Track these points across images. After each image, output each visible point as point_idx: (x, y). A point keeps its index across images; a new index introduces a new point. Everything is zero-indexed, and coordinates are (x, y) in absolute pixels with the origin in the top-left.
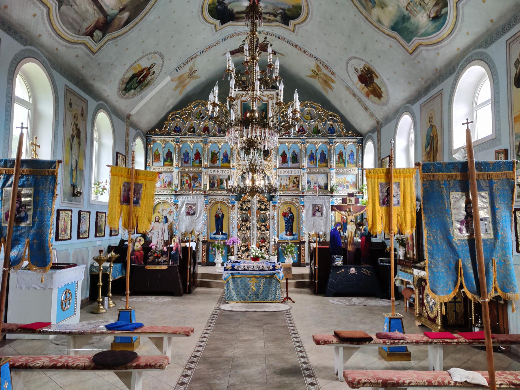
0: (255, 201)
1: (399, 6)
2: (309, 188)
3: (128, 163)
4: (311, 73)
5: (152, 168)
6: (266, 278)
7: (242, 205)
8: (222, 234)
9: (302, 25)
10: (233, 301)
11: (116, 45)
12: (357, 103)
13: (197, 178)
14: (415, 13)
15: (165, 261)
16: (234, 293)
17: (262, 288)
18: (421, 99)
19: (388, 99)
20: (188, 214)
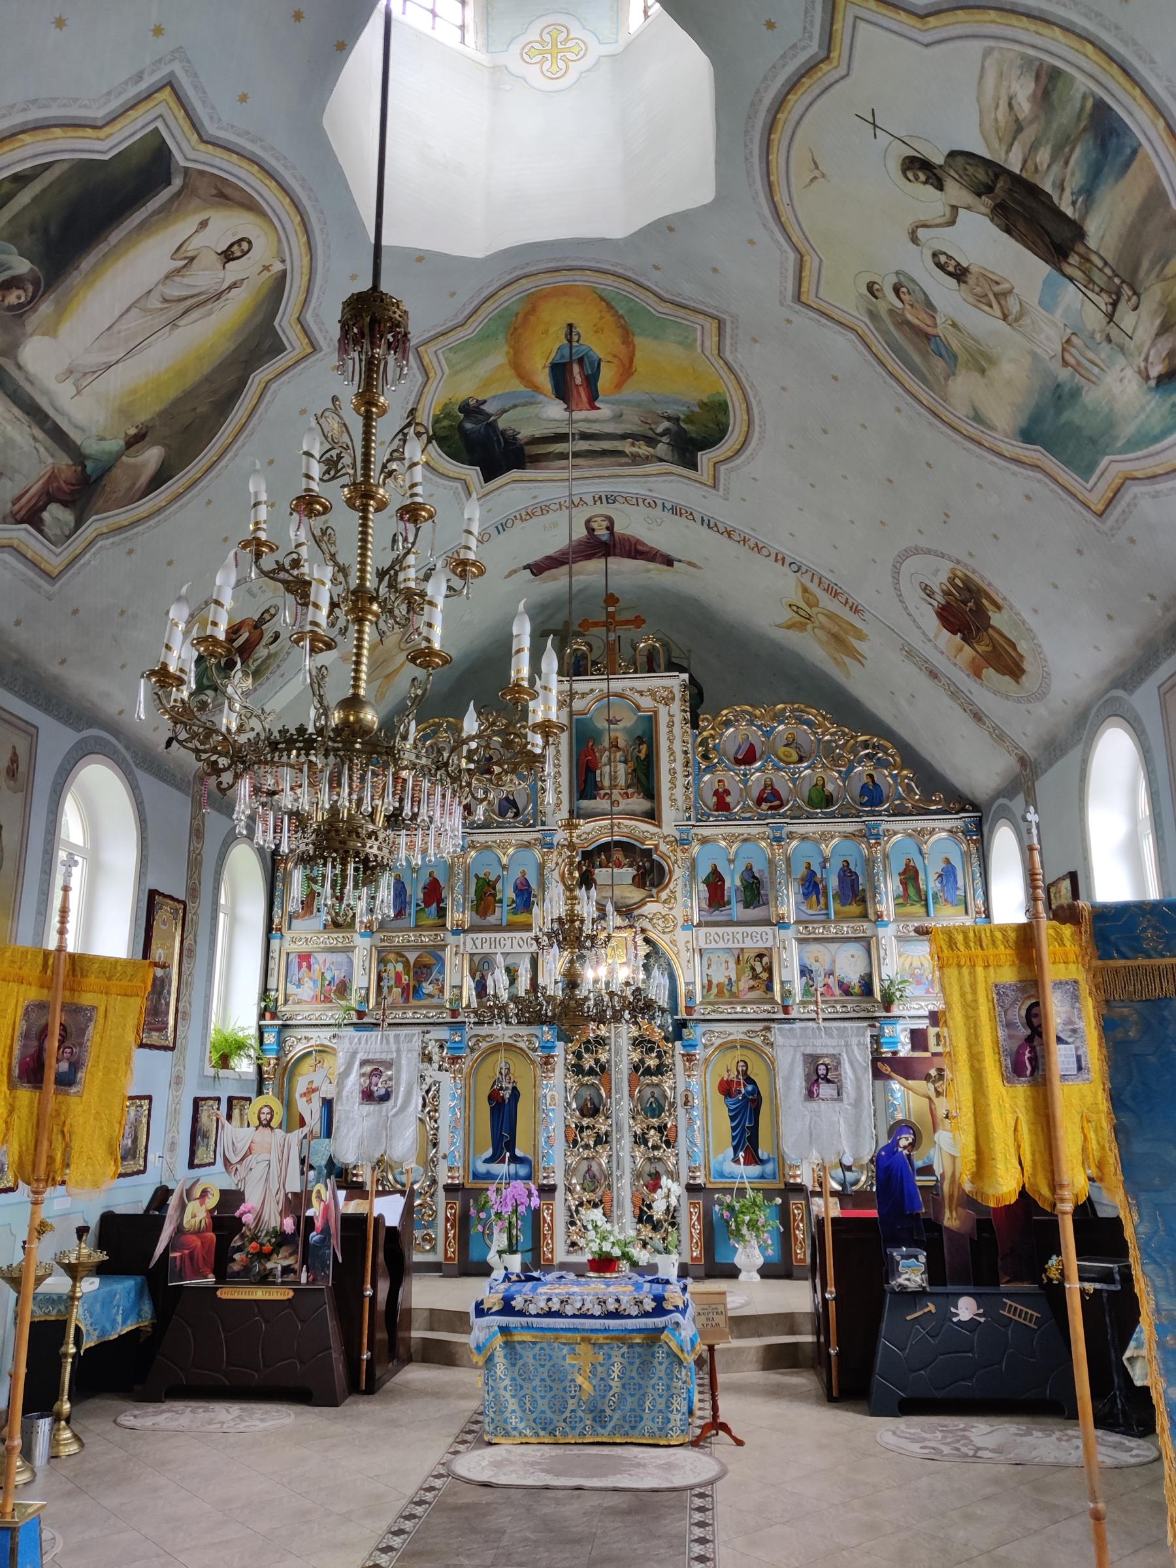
0: (625, 1043)
1: (1034, 355)
2: (806, 992)
3: (195, 924)
4: (788, 615)
5: (288, 935)
6: (631, 1346)
7: (579, 1056)
8: (515, 1159)
9: (738, 462)
10: (507, 1434)
11: (131, 552)
12: (946, 700)
13: (428, 967)
14: (1096, 370)
15: (286, 1270)
16: (512, 1404)
17: (616, 1384)
18: (1156, 667)
19: (1046, 676)
20: (368, 1096)
